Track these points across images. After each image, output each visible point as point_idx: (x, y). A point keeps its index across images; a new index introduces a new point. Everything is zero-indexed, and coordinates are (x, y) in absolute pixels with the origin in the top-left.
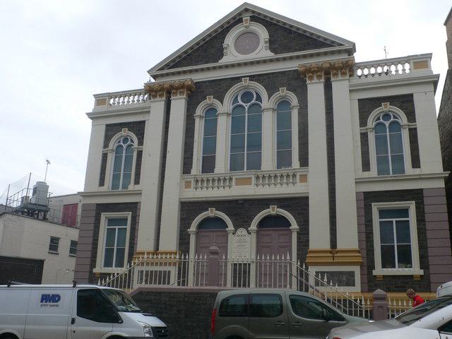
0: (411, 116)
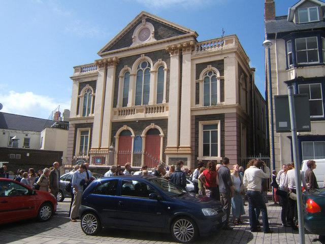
0: (222, 73)
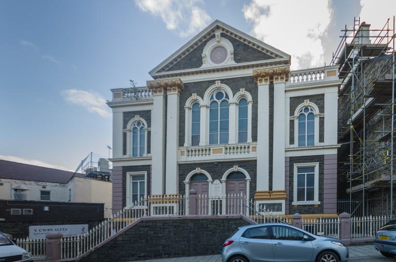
0: (322, 109)
